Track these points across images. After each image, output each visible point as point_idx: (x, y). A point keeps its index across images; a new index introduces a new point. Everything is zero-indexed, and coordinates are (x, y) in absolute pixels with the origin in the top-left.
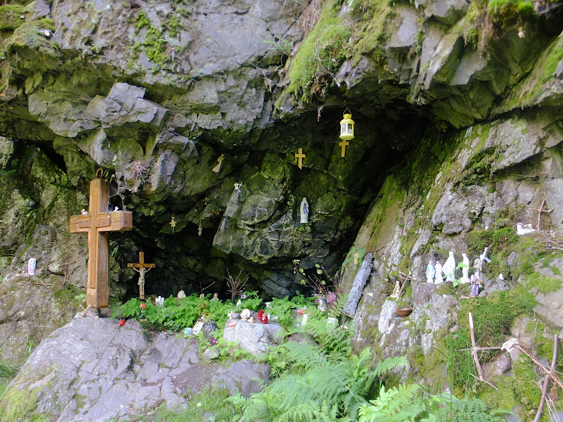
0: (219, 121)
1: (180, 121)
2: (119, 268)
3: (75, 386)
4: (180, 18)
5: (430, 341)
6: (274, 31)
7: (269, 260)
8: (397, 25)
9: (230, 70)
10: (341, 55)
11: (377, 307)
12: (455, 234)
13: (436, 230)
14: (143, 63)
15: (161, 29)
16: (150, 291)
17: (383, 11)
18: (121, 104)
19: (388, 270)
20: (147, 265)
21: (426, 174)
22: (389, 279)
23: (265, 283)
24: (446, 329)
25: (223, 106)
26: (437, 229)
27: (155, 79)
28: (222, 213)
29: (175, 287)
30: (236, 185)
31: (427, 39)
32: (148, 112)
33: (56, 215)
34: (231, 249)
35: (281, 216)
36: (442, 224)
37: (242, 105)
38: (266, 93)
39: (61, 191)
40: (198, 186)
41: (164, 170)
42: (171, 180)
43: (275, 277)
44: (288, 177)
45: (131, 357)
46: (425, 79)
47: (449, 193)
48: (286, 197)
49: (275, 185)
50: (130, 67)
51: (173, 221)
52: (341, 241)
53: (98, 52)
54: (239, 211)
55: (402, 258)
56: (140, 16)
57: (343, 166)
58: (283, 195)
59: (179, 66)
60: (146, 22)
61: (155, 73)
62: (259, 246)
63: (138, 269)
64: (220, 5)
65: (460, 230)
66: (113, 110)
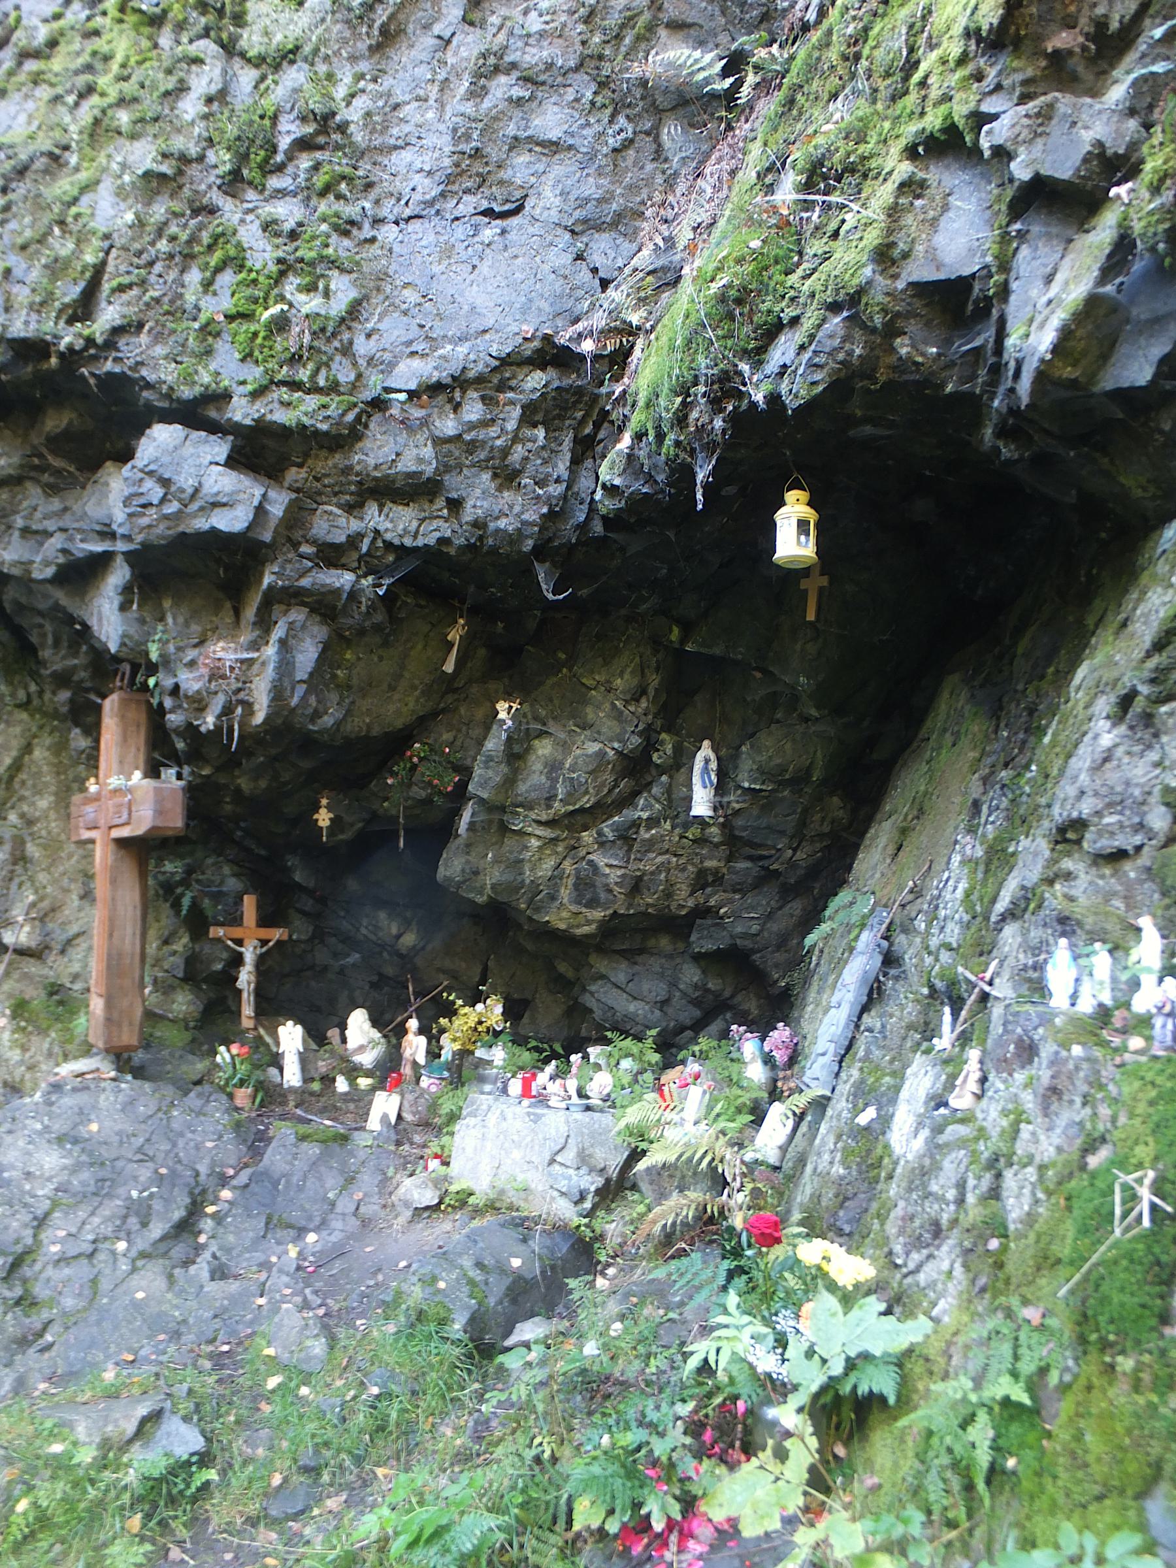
0: (441, 523)
1: (332, 524)
2: (185, 940)
3: (26, 1271)
4: (328, 236)
5: (1027, 1191)
6: (597, 259)
7: (603, 923)
8: (931, 213)
9: (471, 374)
10: (769, 312)
11: (894, 1074)
12: (1120, 855)
13: (1066, 841)
14: (227, 367)
15: (273, 268)
16: (272, 1008)
17: (890, 173)
18: (165, 482)
19: (929, 960)
20: (264, 933)
21: (1051, 670)
22: (932, 987)
23: (593, 988)
24: (1076, 1156)
25: (450, 480)
26: (1069, 834)
27: (258, 409)
28: (462, 786)
29: (343, 998)
30: (502, 707)
31: (1025, 251)
32: (232, 500)
33: (27, 793)
34: (488, 890)
35: (636, 794)
36: (1079, 824)
37: (507, 477)
38: (575, 440)
39: (41, 727)
40: (397, 709)
41: (285, 665)
42: (307, 692)
43: (620, 974)
44: (654, 680)
45: (191, 1193)
46: (1017, 375)
47: (1103, 724)
48: (648, 739)
49: (614, 706)
50: (188, 379)
51: (323, 811)
52: (813, 872)
53: (100, 340)
54: (510, 782)
55: (968, 926)
56: (216, 238)
57: (812, 648)
58: (640, 734)
59: (323, 372)
60: (232, 252)
61: (256, 395)
62: (571, 881)
63: (240, 942)
64: (443, 195)
65: (1138, 839)
66: (142, 501)
